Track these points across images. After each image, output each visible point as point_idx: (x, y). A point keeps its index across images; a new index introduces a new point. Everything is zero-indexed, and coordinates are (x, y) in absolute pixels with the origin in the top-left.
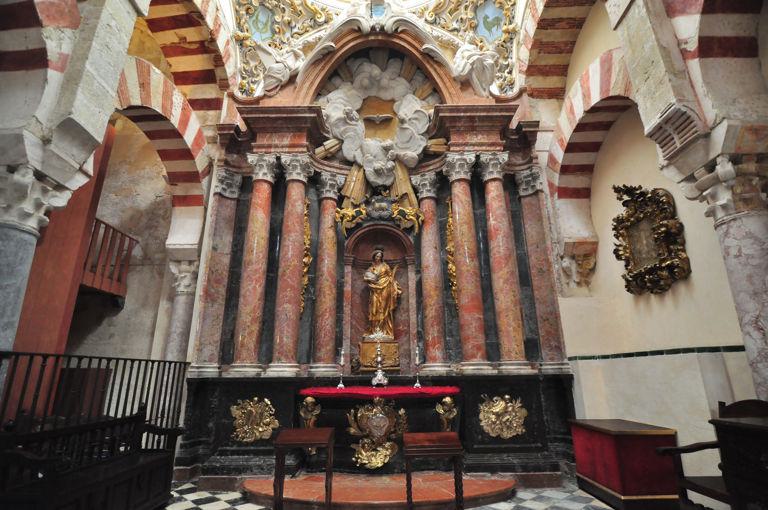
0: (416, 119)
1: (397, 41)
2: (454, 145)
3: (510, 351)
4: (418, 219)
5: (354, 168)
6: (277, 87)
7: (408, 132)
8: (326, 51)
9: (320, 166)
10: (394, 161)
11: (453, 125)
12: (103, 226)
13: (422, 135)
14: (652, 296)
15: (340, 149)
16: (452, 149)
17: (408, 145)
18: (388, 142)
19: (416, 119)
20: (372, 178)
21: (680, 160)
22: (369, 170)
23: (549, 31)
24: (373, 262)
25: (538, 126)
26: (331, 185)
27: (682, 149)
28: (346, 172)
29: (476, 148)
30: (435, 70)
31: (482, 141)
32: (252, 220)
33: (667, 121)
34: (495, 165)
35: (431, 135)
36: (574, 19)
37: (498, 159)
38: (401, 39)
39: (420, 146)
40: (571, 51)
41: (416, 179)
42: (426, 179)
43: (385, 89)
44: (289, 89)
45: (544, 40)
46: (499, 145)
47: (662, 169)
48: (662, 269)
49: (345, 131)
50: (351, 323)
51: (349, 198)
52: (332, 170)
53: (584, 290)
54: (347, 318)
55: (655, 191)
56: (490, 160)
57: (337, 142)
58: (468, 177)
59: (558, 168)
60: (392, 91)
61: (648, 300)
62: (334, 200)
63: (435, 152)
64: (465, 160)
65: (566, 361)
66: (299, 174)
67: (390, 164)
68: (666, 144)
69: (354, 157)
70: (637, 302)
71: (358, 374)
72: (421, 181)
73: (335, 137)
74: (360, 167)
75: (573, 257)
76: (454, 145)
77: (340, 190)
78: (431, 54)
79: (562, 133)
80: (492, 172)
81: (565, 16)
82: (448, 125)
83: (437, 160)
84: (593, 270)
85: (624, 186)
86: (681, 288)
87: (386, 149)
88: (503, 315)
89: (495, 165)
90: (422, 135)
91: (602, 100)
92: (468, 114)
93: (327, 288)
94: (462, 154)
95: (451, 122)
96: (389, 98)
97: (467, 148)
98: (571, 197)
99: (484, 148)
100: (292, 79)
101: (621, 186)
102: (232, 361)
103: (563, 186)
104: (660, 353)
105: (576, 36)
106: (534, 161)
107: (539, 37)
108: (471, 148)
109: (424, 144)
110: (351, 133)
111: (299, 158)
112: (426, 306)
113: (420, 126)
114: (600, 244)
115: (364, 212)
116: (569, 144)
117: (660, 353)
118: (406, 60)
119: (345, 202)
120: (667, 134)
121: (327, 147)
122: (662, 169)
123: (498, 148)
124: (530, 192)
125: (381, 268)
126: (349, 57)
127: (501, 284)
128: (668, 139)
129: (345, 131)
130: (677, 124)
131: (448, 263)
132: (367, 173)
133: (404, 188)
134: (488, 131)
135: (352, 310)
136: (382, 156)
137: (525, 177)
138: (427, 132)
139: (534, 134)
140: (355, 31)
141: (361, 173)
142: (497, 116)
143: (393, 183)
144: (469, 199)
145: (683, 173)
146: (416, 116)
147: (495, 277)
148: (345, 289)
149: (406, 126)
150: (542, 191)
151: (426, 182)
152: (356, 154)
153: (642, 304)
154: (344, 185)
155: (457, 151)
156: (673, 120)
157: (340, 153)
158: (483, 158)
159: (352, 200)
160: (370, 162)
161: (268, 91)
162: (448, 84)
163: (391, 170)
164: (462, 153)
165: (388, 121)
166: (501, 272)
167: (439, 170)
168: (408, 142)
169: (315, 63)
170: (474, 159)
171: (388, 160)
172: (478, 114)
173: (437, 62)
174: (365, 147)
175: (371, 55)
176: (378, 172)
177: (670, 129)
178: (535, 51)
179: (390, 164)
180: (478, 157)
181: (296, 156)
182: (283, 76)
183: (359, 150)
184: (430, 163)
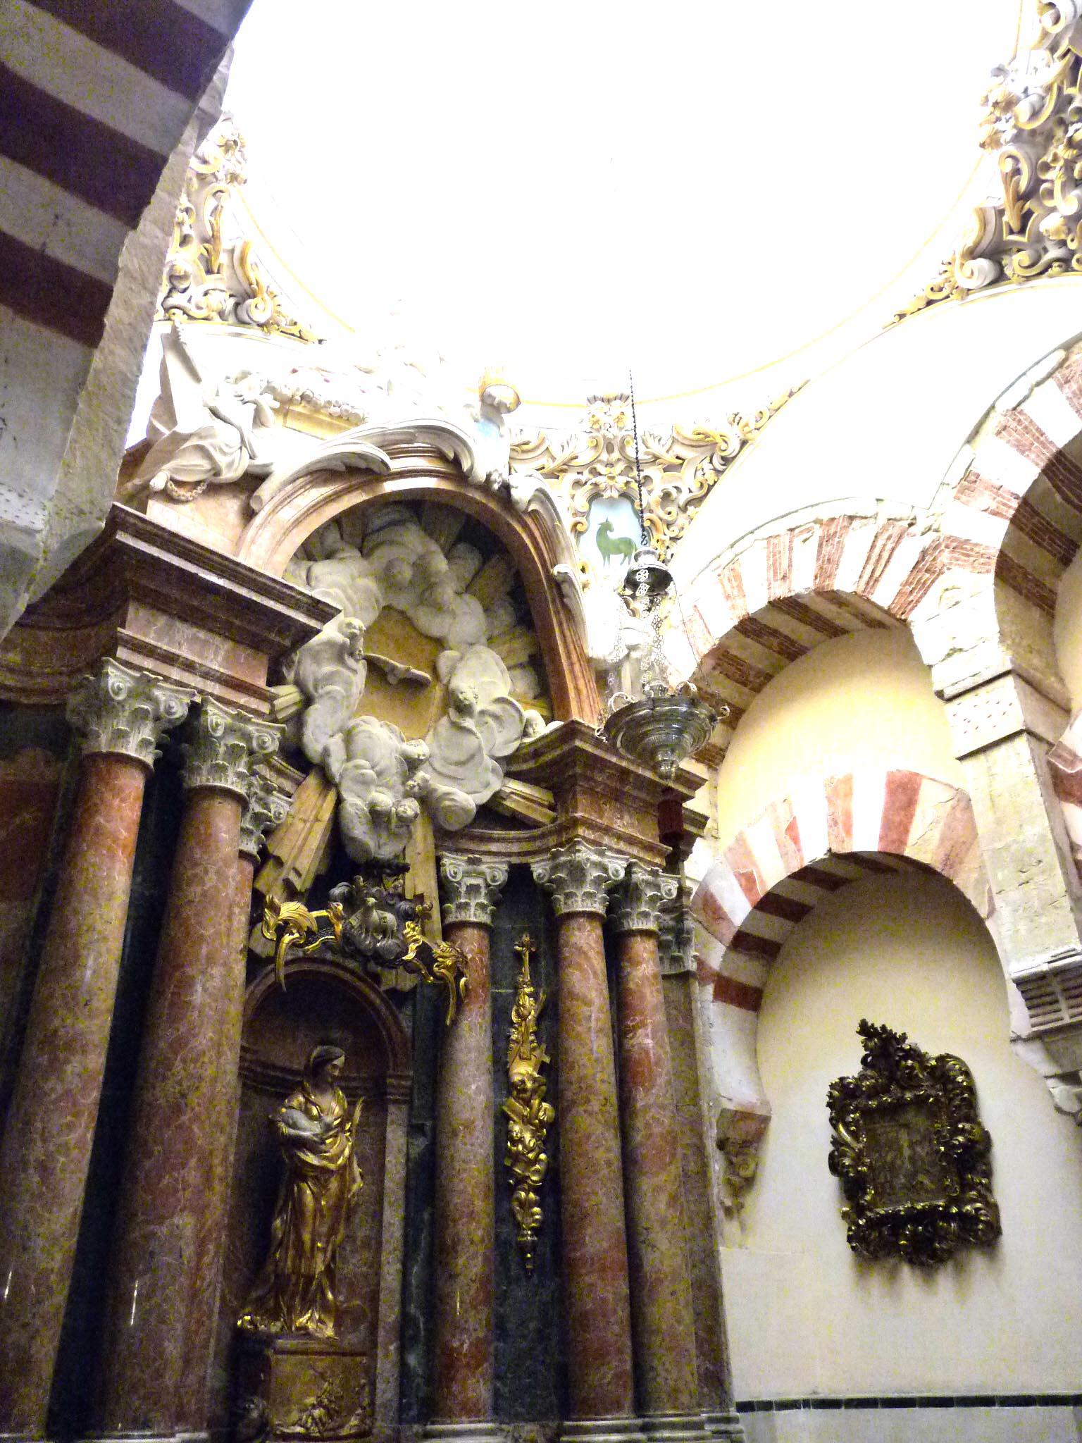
0: (496, 717)
1: (519, 529)
3: (676, 1390)
4: (457, 979)
5: (312, 781)
6: (198, 483)
7: (470, 743)
8: (363, 465)
12: (273, 966)
13: (498, 759)
14: (906, 1271)
17: (459, 772)
18: (418, 749)
19: (496, 717)
20: (359, 830)
21: (1059, 1043)
22: (355, 804)
23: (749, 641)
24: (316, 1076)
27: (1071, 1027)
30: (560, 625)
32: (95, 894)
33: (1057, 973)
35: (515, 768)
36: (793, 642)
37: (658, 887)
38: (525, 526)
39: (487, 785)
40: (757, 690)
41: (454, 865)
43: (438, 608)
44: (231, 506)
45: (734, 652)
47: (1014, 1041)
48: (946, 1216)
49: (329, 678)
55: (942, 1059)
56: (648, 883)
59: (729, 935)
60: (448, 620)
61: (893, 1275)
63: (514, 812)
65: (733, 1412)
68: (1038, 1006)
70: (962, 1293)
72: (467, 874)
73: (298, 683)
74: (328, 782)
78: (565, 588)
80: (645, 915)
81: (785, 631)
82: (578, 770)
84: (750, 1182)
85: (883, 1027)
86: (978, 1262)
87: (412, 764)
88: (664, 1290)
89: (653, 900)
90: (498, 759)
91: (880, 852)
95: (586, 765)
96: (435, 631)
100: (252, 481)
101: (878, 1025)
102: (648, 1408)
103: (726, 974)
104: (987, 1401)
105: (778, 668)
107: (728, 643)
109: (496, 785)
110: (337, 688)
112: (460, 1241)
113: (500, 738)
114: (774, 1125)
116: (769, 895)
117: (987, 1401)
118: (343, 469)
120: (1049, 990)
122: (1014, 1041)
123: (657, 860)
125: (332, 1106)
126: (517, 574)
128: (1048, 999)
129: (329, 678)
130: (1071, 984)
131: (508, 1118)
133: (420, 881)
134: (642, 810)
136: (396, 780)
138: (507, 760)
140: (441, 456)
141: (331, 798)
145: (1061, 1066)
146: (496, 708)
149: (468, 723)
153: (876, 1282)
155: (287, 707)
156: (1069, 976)
160: (365, 782)
161: (179, 484)
162: (577, 667)
165: (413, 686)
166: (663, 1177)
168: (461, 764)
169: (322, 473)
171: (407, 795)
173: (565, 606)
174: (360, 741)
175: (493, 561)
176: (377, 817)
177: (1056, 987)
178: (711, 662)
180: (196, 710)
182: (230, 465)
183: (339, 738)
184: (497, 833)
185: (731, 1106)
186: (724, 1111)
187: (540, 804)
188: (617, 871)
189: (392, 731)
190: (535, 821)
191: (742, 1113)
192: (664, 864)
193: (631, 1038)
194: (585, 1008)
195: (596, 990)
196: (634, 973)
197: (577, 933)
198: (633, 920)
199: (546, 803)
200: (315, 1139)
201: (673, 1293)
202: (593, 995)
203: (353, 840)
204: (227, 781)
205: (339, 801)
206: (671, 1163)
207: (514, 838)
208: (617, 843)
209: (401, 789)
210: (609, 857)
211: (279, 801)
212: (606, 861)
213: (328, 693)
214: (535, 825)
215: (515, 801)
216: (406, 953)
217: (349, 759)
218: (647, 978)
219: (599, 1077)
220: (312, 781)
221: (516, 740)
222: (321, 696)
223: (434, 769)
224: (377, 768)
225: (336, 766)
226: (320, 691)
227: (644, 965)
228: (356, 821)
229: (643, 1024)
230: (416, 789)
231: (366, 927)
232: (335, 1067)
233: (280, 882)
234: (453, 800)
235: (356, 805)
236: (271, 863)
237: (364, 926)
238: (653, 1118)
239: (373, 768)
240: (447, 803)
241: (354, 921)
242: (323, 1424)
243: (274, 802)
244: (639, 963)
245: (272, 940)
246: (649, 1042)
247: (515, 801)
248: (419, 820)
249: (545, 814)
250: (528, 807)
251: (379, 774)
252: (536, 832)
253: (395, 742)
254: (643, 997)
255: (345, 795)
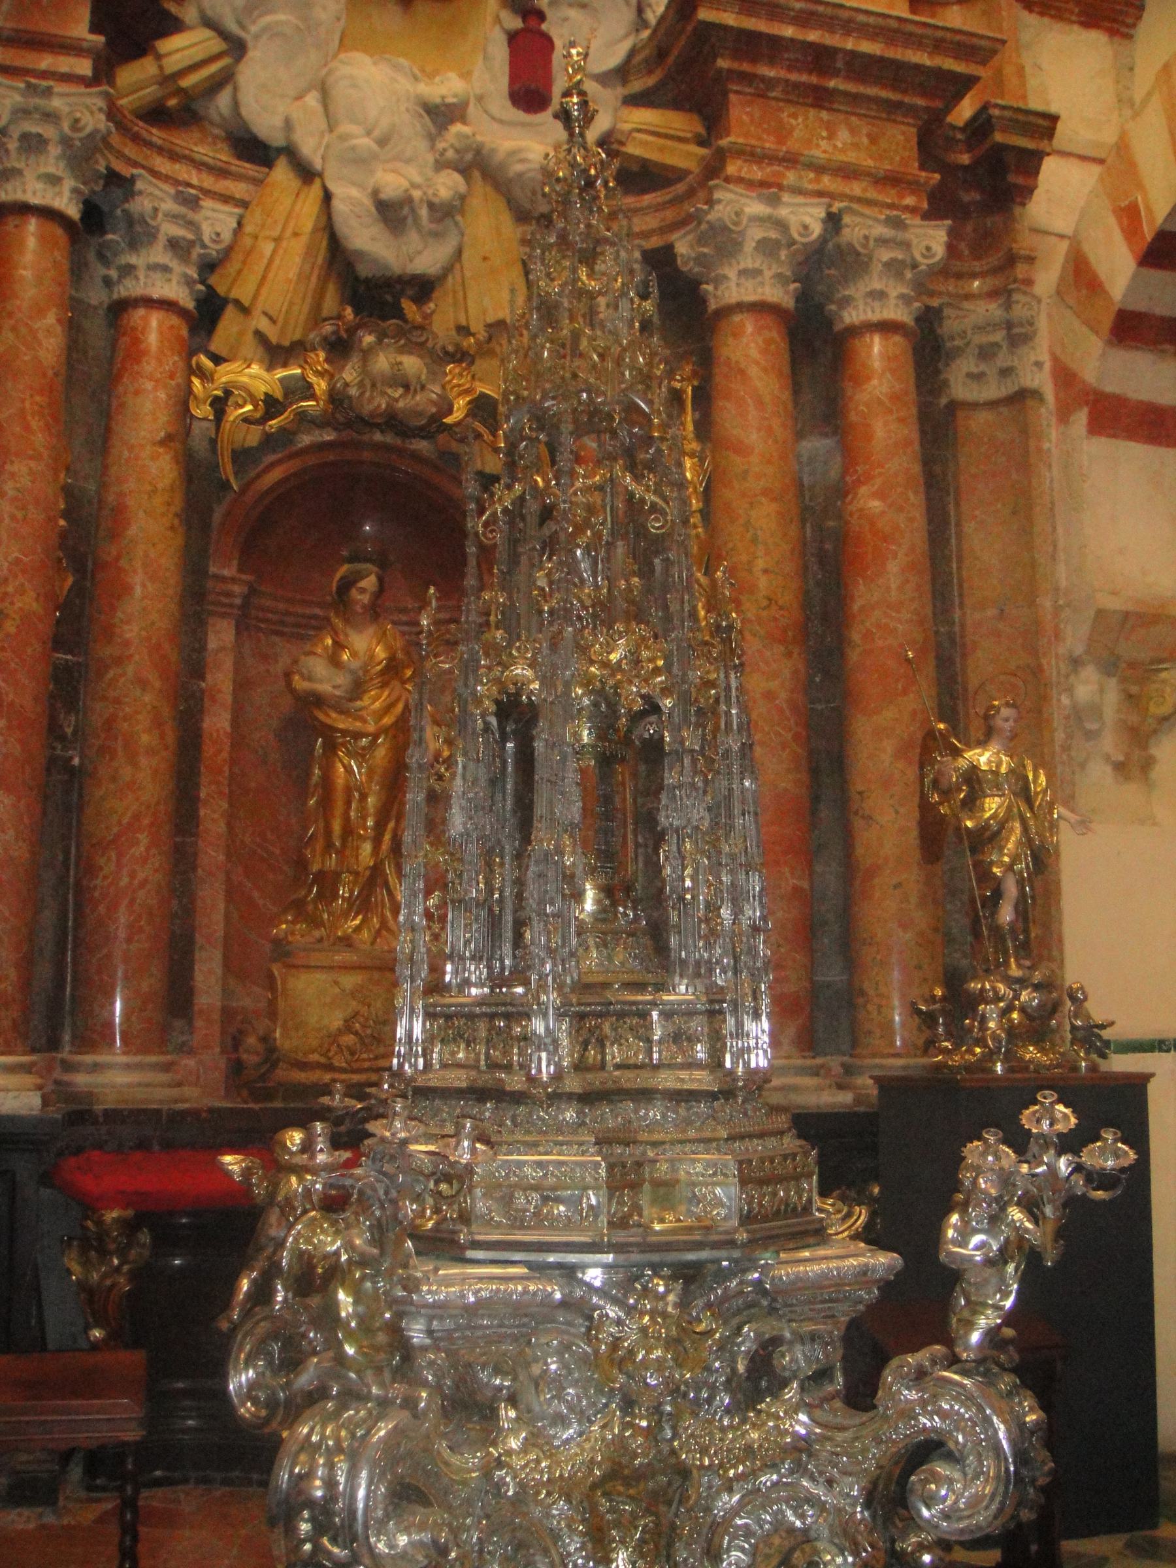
2: (741, 153)
5: (281, 173)
9: (130, 150)
10: (464, 171)
11: (746, 67)
15: (225, 79)
16: (731, 169)
25: (1050, 133)
26: (174, 244)
28: (239, 189)
29: (827, 182)
31: (851, 157)
34: (894, 268)
37: (907, 245)
42: (50, 117)
46: (913, 186)
50: (228, 880)
51: (245, 310)
52: (182, 171)
53: (1131, 793)
54: (211, 855)
56: (883, 242)
57: (216, 45)
58: (789, 302)
59: (1107, 322)
62: (182, 312)
64: (781, 225)
66: (53, 180)
67: (447, 185)
69: (288, 125)
71: (269, 1095)
74: (306, 174)
75: (1110, 666)
76: (741, 153)
77: (209, 267)
79: (1140, 186)
80: (881, 295)
83: (648, 199)
92: (813, 36)
93: (144, 720)
94: (774, 201)
97: (791, 177)
98: (1132, 434)
99: (856, 188)
106: (1021, 270)
108: (808, 179)
111: (56, 103)
115: (321, 386)
119: (229, 324)
121: (173, 64)
123: (910, 201)
124: (993, 390)
127: (886, 758)
132: (338, 205)
135: (231, 819)
137: (979, 328)
138: (622, 73)
139: (1031, 162)
141: (315, 192)
142: (918, 67)
143: (448, 270)
144: (786, 395)
147: (862, 727)
148: (207, 723)
150: (1035, 394)
151: (48, 131)
152: (296, 115)
154: (229, 251)
155: (750, 184)
157: (223, 100)
158: (855, 230)
159: (263, 324)
160: (362, 161)
163: (445, 212)
164: (769, 189)
166: (889, 714)
167: (655, 242)
170: (817, 229)
172: (849, 45)
174: (341, 92)
179: (447, 185)
180: (833, 221)
181: (48, 92)
183: (312, 100)
185: (1114, 604)
186: (1101, 613)
187: (680, 139)
188: (806, 227)
189: (397, 67)
190: (674, 169)
191: (1139, 615)
192: (925, 206)
193: (851, 502)
194: (738, 460)
195: (759, 430)
196: (857, 397)
197: (730, 340)
198: (856, 308)
199: (689, 135)
200: (337, 693)
201: (897, 886)
202: (753, 438)
203: (360, 254)
204: (24, 191)
205: (327, 197)
206: (905, 692)
207: (649, 207)
208: (817, 181)
209: (430, 158)
210: (789, 205)
211: (215, 215)
212: (783, 212)
213: (265, 29)
214: (679, 175)
215: (645, 144)
216: (450, 411)
217: (331, 129)
218: (880, 402)
219: (761, 563)
220: (281, 173)
221: (627, 35)
222: (257, 37)
223: (493, 118)
224: (377, 133)
225: (309, 147)
226: (254, 29)
227: (875, 382)
228: (354, 222)
229: (868, 478)
230: (450, 154)
231: (372, 382)
232: (363, 591)
233: (249, 337)
234: (522, 161)
235: (350, 198)
236: (230, 312)
237: (368, 383)
238: (878, 626)
239: (368, 133)
240: (519, 168)
241: (349, 374)
242: (353, 1053)
243: (207, 218)
244: (869, 379)
245: (205, 419)
246: (875, 505)
247: (645, 144)
248: (475, 202)
249: (689, 154)
250: (661, 149)
251: (383, 142)
252: (680, 188)
253: (405, 85)
254: (869, 437)
255: (332, 186)
